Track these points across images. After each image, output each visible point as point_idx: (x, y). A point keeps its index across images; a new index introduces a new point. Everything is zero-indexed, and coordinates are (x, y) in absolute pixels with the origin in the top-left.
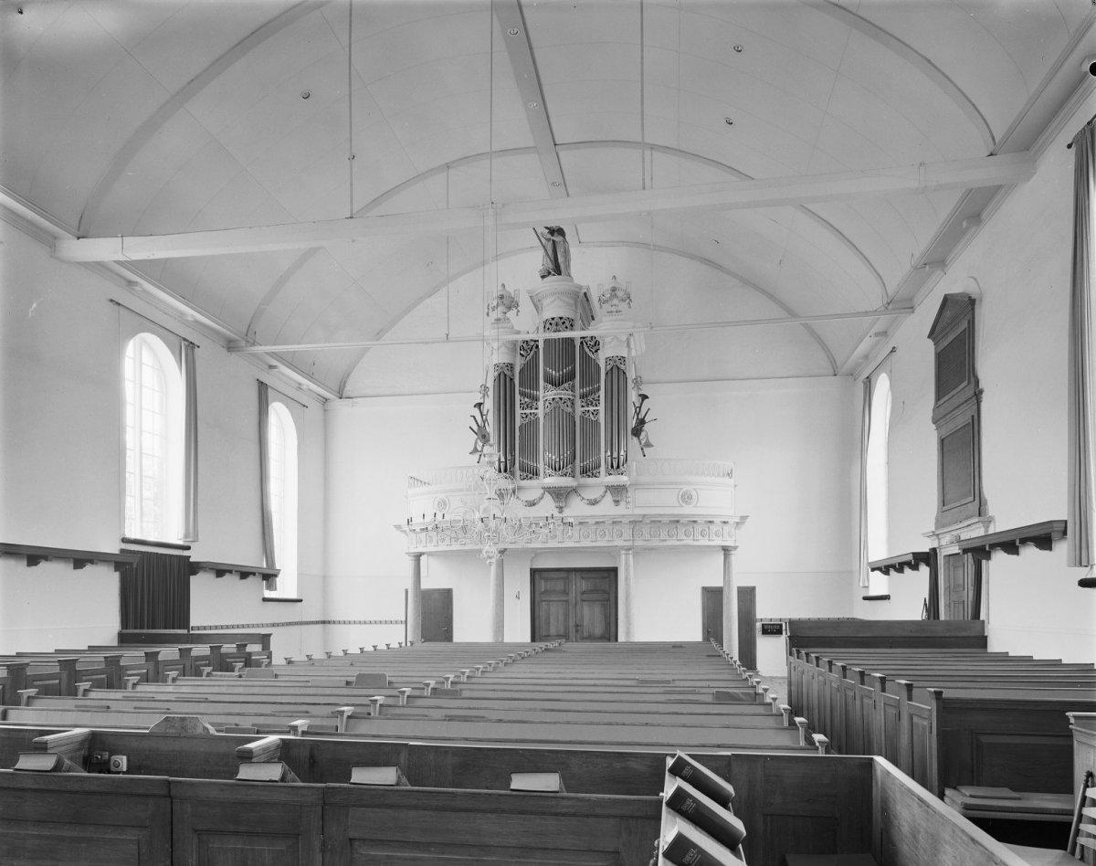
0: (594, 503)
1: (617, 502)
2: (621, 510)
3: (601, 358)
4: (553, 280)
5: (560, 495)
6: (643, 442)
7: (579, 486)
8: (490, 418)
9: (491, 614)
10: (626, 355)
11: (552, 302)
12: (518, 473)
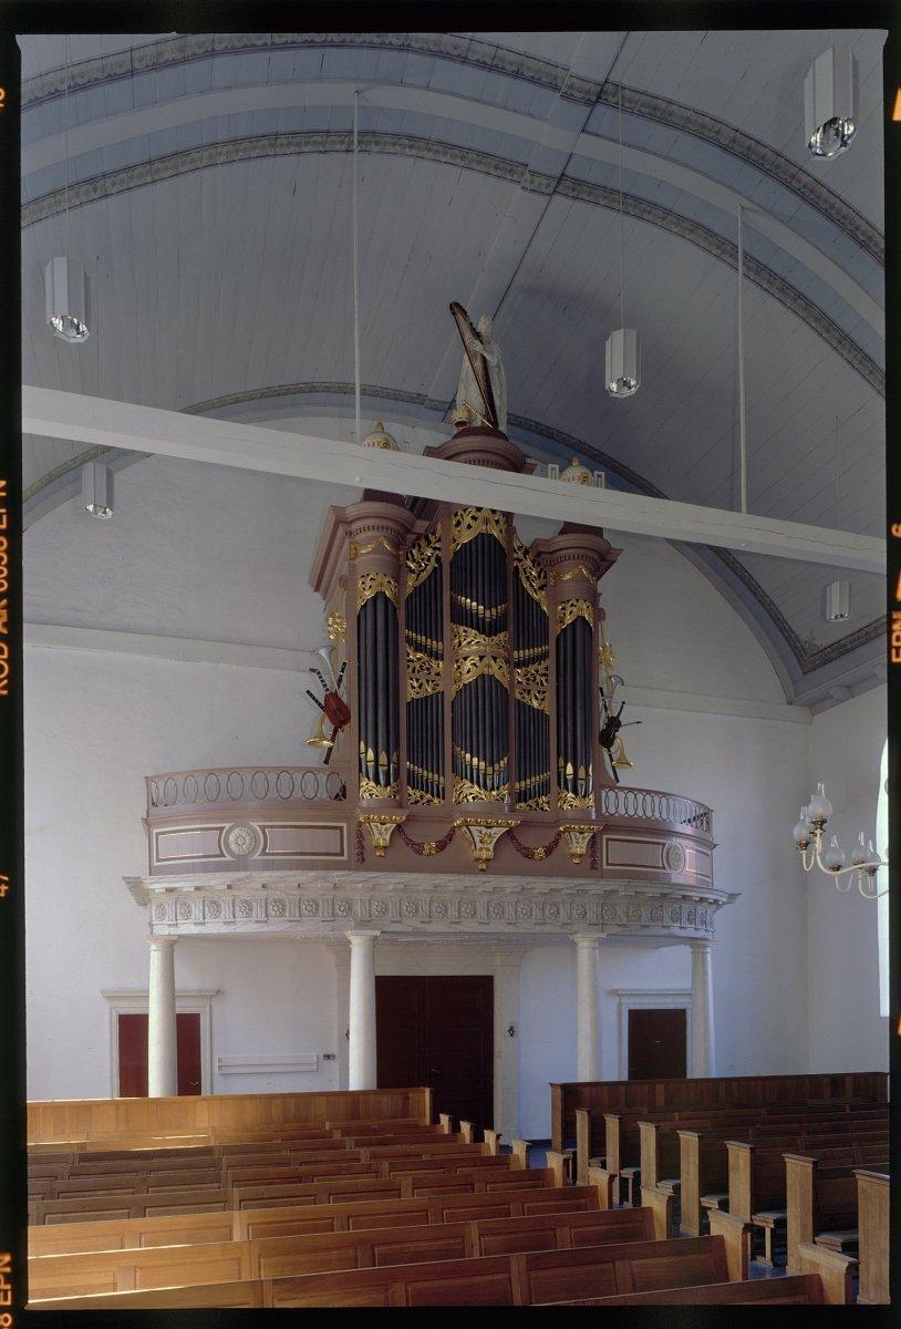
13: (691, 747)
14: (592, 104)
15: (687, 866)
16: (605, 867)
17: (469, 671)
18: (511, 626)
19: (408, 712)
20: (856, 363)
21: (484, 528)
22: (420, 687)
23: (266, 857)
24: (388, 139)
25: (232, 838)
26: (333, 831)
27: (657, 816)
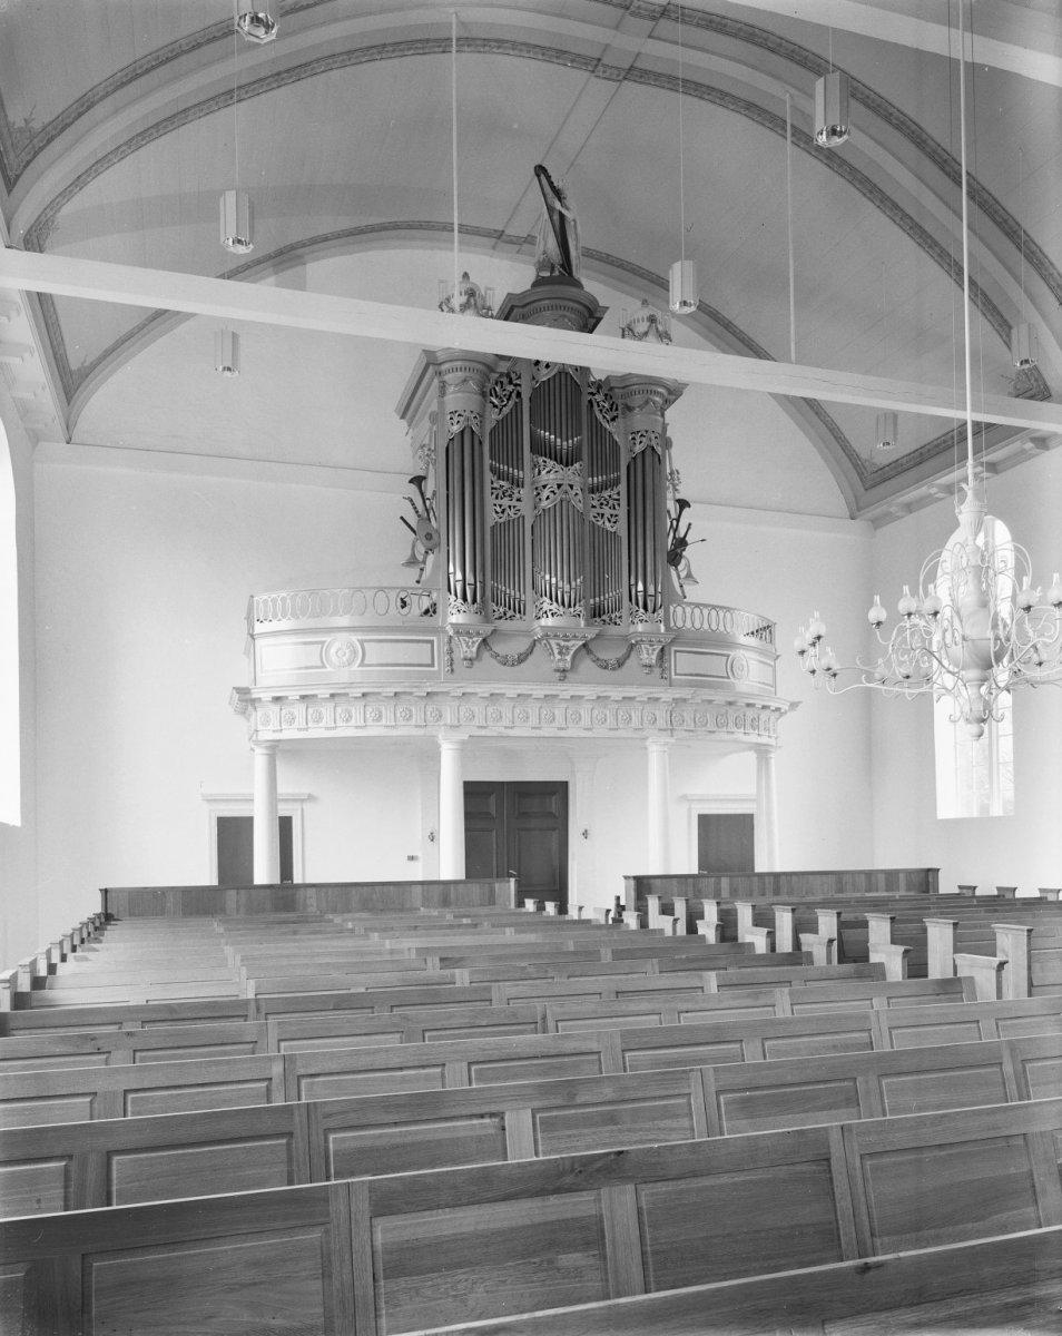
14: (654, 18)
15: (750, 670)
16: (674, 677)
17: (548, 498)
18: (585, 456)
19: (493, 535)
20: (897, 219)
22: (503, 512)
23: (365, 669)
24: (479, 42)
25: (333, 650)
26: (425, 645)
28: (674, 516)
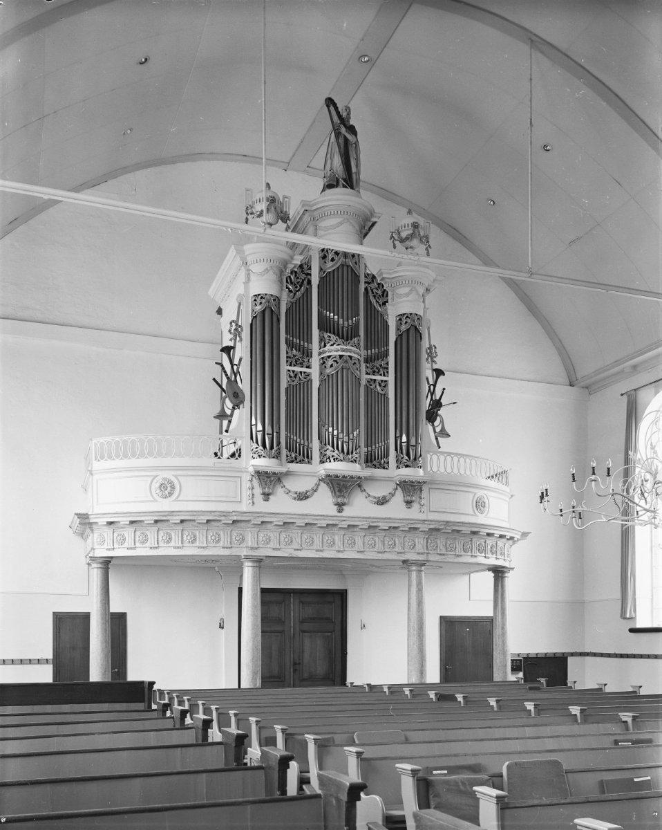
0: (303, 497)
1: (266, 496)
2: (414, 513)
3: (392, 313)
4: (340, 195)
5: (341, 486)
6: (438, 429)
7: (288, 474)
8: (245, 370)
9: (193, 651)
10: (422, 315)
11: (341, 223)
12: (284, 452)
13: (495, 438)
21: (344, 260)
22: (295, 376)
27: (468, 473)
28: (431, 382)
